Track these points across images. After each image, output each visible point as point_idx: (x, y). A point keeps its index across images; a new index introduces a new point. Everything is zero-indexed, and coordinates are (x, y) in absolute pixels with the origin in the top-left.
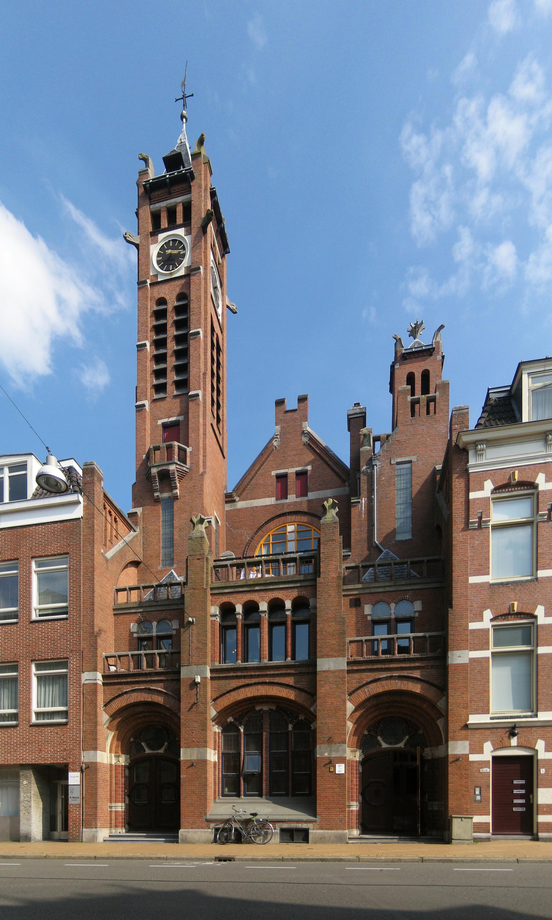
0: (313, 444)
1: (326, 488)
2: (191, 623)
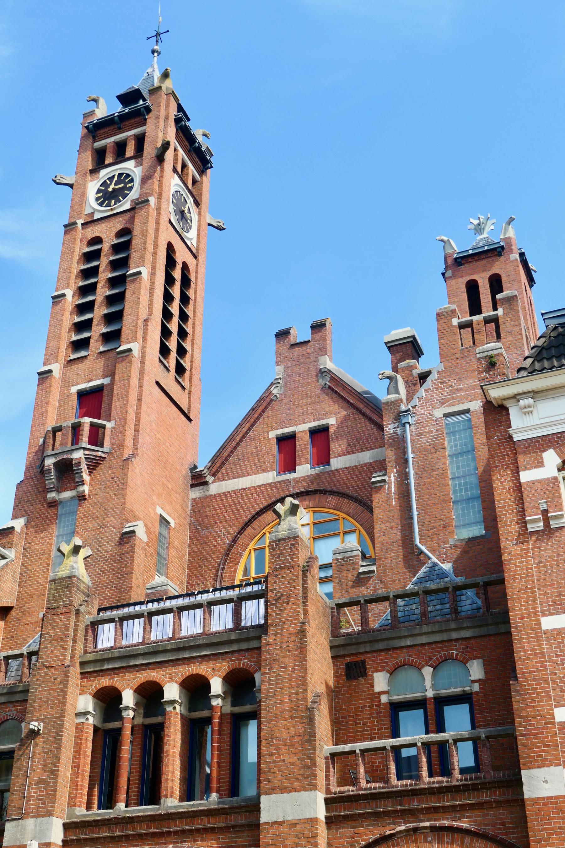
0: (337, 389)
1: (362, 450)
2: (34, 734)
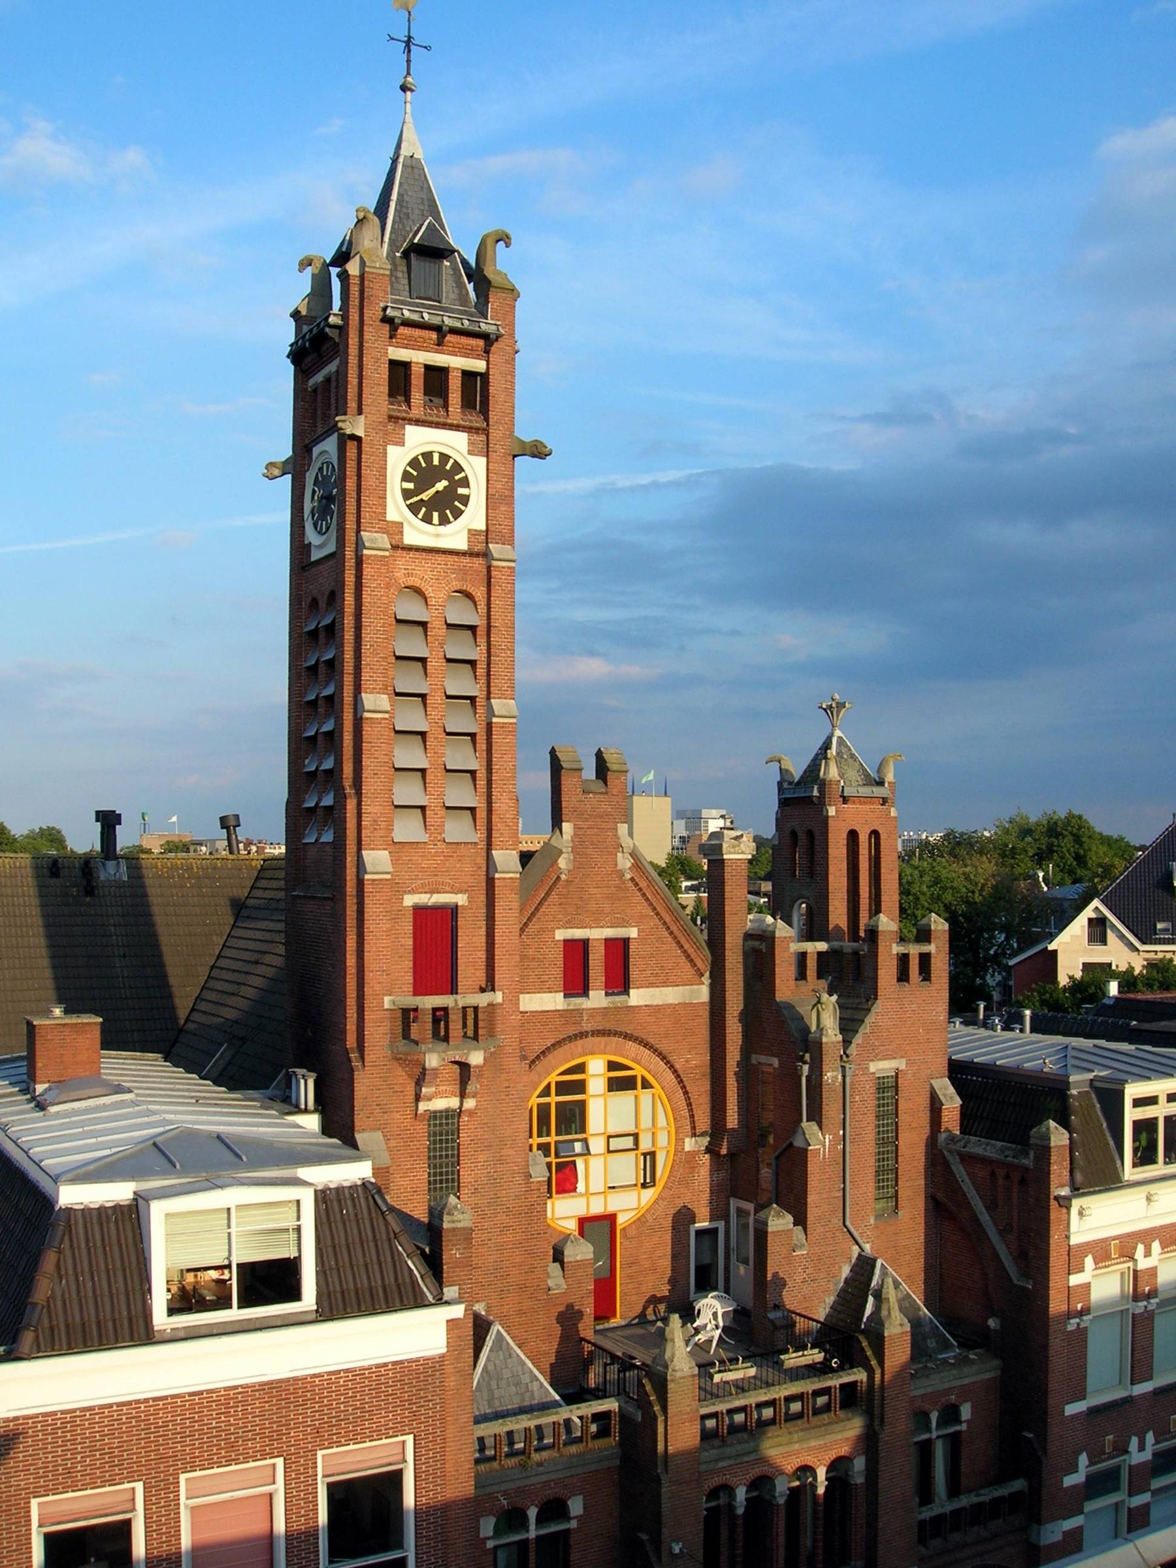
1: (665, 984)
